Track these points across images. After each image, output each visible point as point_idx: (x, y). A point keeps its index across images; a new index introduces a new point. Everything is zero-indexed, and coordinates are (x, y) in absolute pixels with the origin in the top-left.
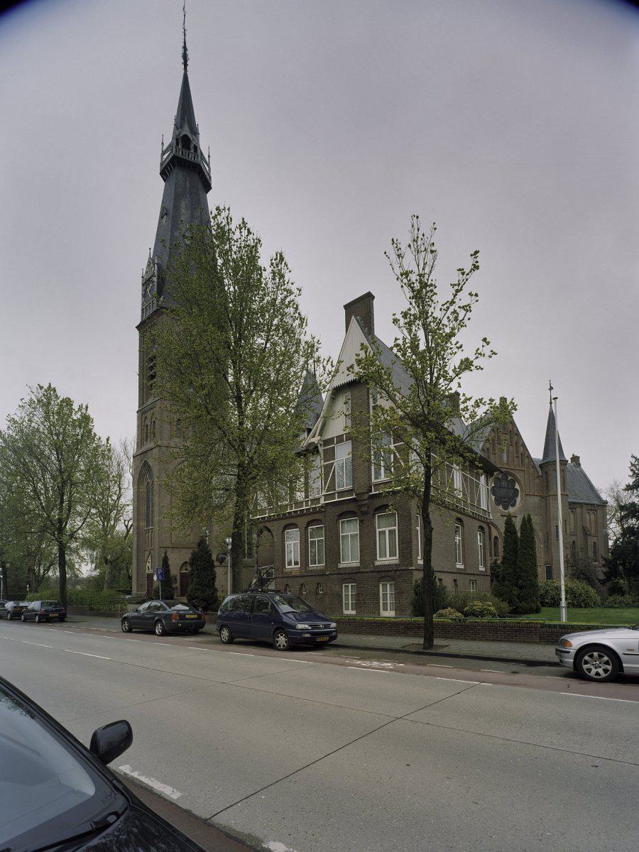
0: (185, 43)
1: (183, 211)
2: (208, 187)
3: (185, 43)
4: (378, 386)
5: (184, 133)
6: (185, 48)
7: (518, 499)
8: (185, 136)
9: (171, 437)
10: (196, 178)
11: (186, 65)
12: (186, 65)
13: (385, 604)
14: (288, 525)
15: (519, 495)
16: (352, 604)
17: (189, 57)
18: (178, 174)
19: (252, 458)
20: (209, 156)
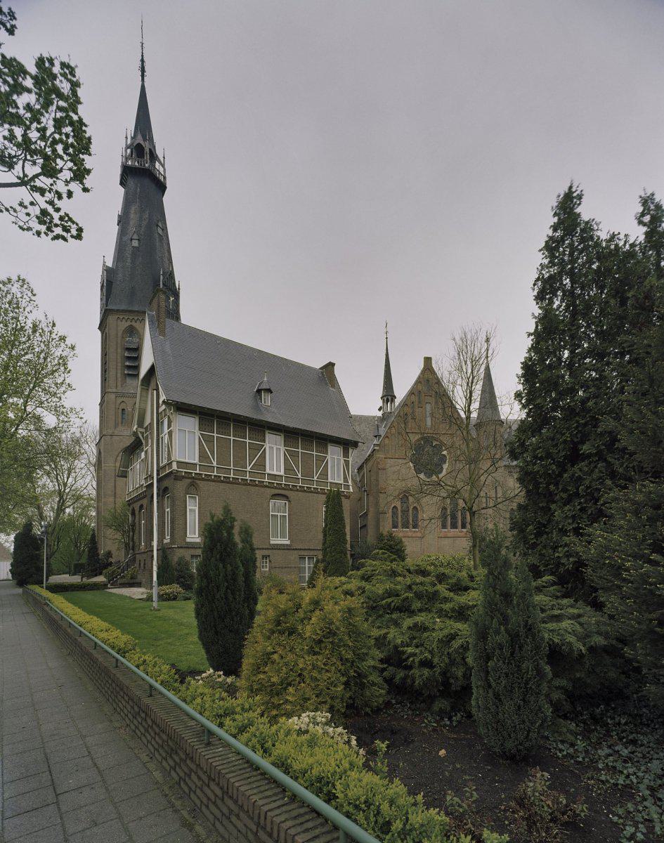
0: (142, 56)
1: (132, 216)
2: (162, 187)
3: (142, 56)
4: (262, 707)
5: (137, 142)
6: (142, 61)
7: (445, 466)
8: (139, 145)
9: (116, 426)
10: (147, 181)
11: (143, 76)
12: (143, 76)
13: (283, 525)
14: (278, 494)
15: (447, 462)
16: (274, 483)
17: (146, 69)
18: (131, 182)
19: (641, 813)
20: (164, 157)
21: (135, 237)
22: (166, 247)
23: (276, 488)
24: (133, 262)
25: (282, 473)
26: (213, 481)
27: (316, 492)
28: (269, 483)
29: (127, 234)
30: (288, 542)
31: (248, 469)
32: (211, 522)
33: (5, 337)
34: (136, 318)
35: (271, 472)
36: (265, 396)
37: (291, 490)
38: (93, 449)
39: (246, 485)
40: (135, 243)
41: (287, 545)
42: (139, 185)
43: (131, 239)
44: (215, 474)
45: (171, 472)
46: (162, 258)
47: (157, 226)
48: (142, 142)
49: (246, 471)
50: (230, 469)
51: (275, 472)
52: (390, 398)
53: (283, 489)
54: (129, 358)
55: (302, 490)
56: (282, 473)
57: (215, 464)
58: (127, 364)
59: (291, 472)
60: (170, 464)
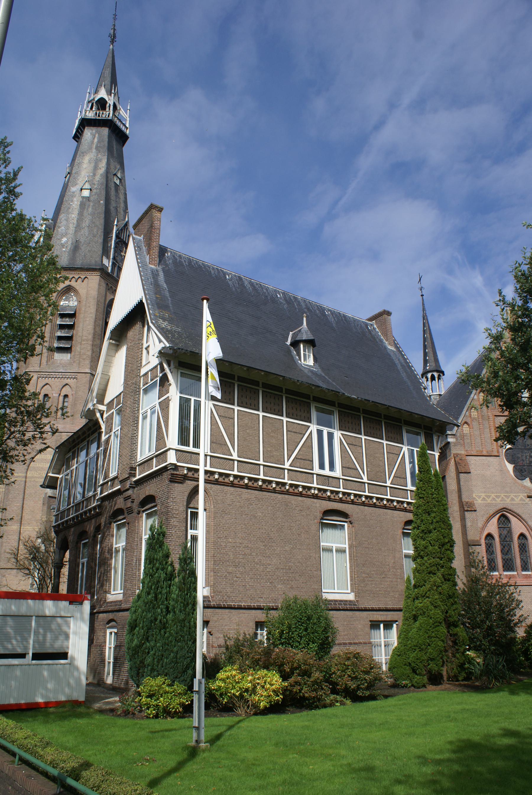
0: (423, 304)
21: (87, 186)
22: (122, 197)
23: (329, 499)
24: (81, 214)
25: (338, 473)
26: (232, 485)
27: (389, 506)
28: (320, 490)
29: (77, 184)
30: (351, 597)
31: (287, 465)
32: (425, 677)
33: (10, 425)
34: (77, 277)
35: (322, 472)
36: (304, 351)
37: (353, 502)
38: (71, 226)
39: (282, 493)
40: (86, 193)
41: (350, 601)
42: (97, 135)
43: (81, 189)
44: (236, 472)
45: (165, 468)
46: (116, 208)
47: (115, 175)
48: (106, 97)
49: (284, 469)
50: (259, 465)
51: (327, 472)
52: (436, 374)
53: (341, 501)
54: (62, 327)
55: (368, 503)
56: (338, 473)
57: (235, 456)
58: (59, 334)
59: (352, 472)
60: (162, 455)
